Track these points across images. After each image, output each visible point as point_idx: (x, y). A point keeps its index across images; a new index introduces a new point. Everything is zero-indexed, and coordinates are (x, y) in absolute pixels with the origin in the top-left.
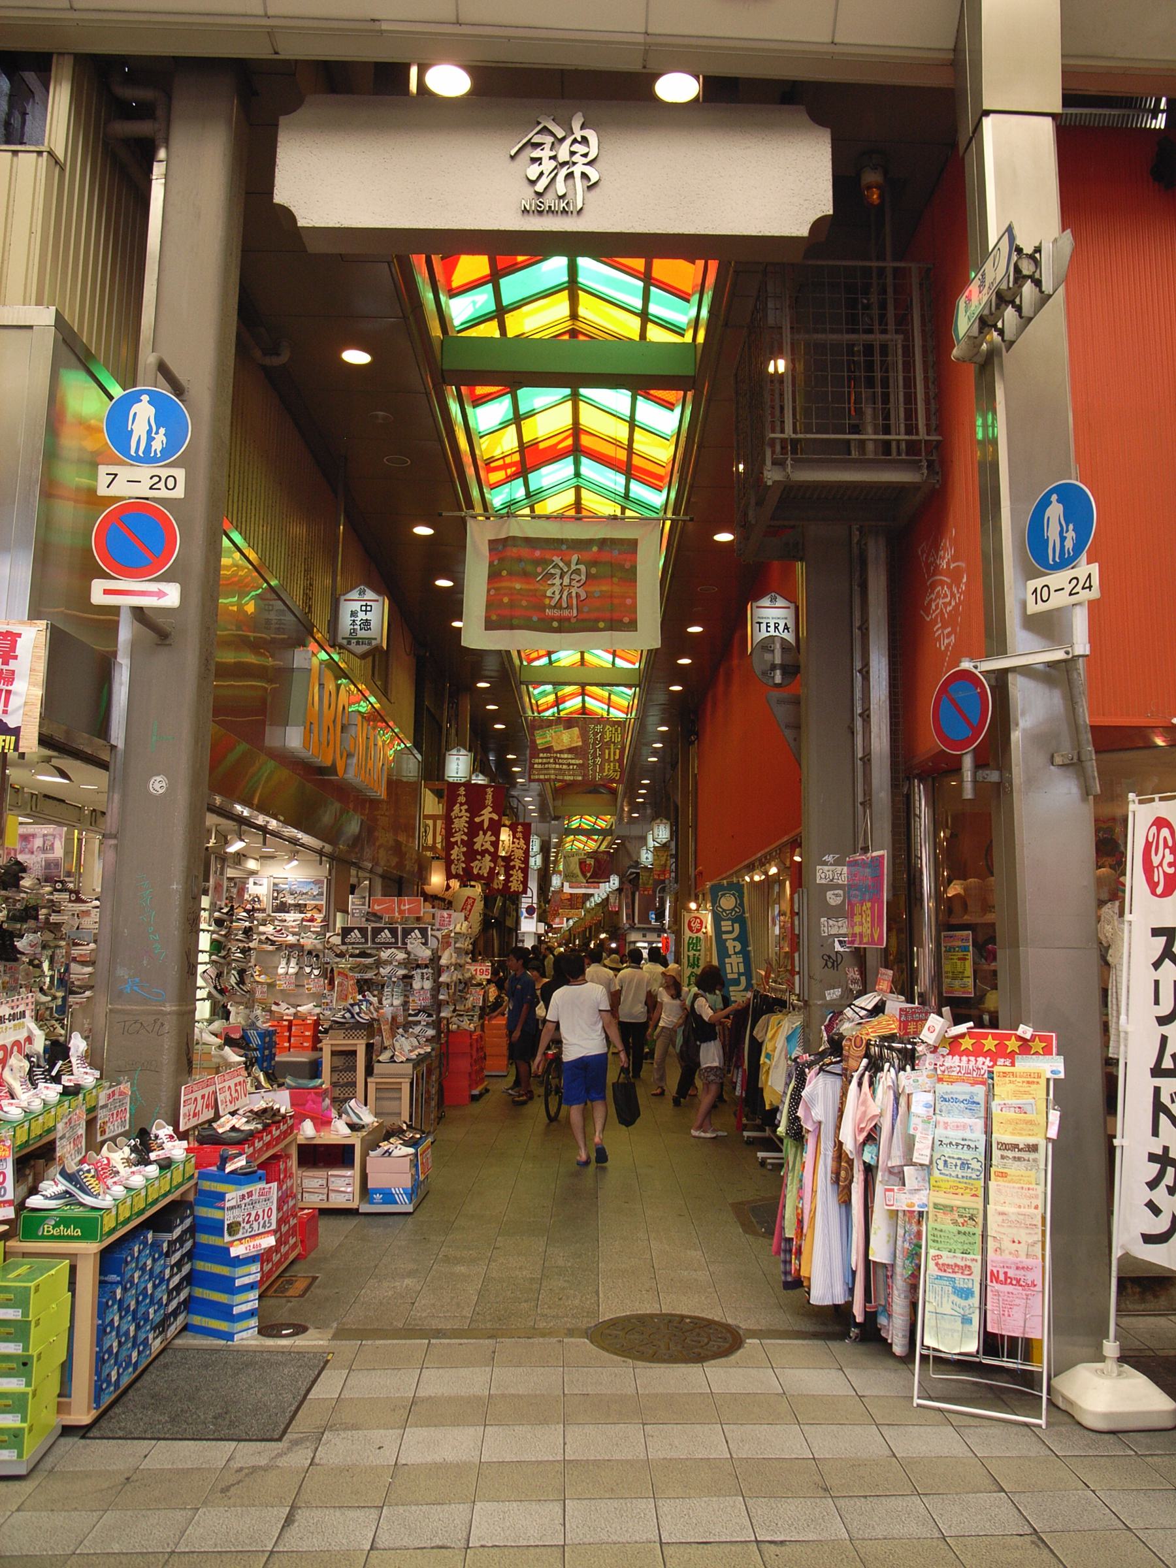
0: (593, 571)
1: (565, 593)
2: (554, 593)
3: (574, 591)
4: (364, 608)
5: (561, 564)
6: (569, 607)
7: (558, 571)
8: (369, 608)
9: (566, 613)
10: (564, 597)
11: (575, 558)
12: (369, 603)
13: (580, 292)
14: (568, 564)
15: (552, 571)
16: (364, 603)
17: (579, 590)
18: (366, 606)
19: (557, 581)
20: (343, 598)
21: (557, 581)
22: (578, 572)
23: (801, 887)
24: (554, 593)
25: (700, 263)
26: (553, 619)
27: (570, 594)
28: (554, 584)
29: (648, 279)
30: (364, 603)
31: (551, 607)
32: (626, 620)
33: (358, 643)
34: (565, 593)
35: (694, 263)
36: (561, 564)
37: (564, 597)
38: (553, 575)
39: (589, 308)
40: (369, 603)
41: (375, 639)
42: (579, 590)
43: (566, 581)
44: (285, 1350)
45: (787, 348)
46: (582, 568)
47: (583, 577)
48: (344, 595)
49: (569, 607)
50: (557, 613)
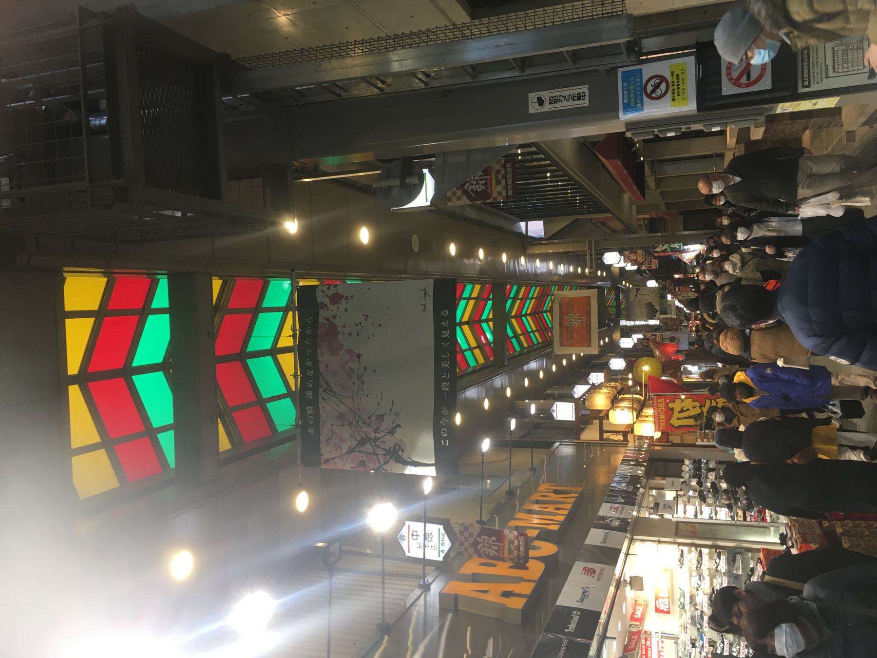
0: (570, 311)
1: (577, 320)
2: (480, 188)
3: (576, 318)
4: (415, 537)
5: (568, 322)
6: (582, 319)
7: (570, 323)
8: (415, 533)
9: (584, 320)
10: (579, 321)
11: (566, 317)
12: (411, 533)
13: (462, 321)
14: (568, 319)
15: (570, 325)
16: (411, 537)
17: (577, 315)
18: (413, 535)
19: (573, 323)
20: (407, 554)
21: (573, 323)
22: (571, 316)
23: (625, 645)
24: (480, 188)
25: (65, 274)
26: (586, 324)
27: (578, 319)
28: (574, 324)
29: (285, 310)
30: (411, 537)
31: (582, 325)
32: (587, 300)
33: (443, 544)
34: (577, 320)
35: (66, 278)
36: (568, 322)
37: (579, 321)
38: (571, 324)
39: (465, 319)
40: (411, 533)
41: (439, 529)
42: (577, 315)
43: (573, 320)
44: (408, 72)
45: (588, 267)
46: (570, 315)
47: (572, 314)
48: (405, 553)
49: (582, 319)
50: (584, 324)
